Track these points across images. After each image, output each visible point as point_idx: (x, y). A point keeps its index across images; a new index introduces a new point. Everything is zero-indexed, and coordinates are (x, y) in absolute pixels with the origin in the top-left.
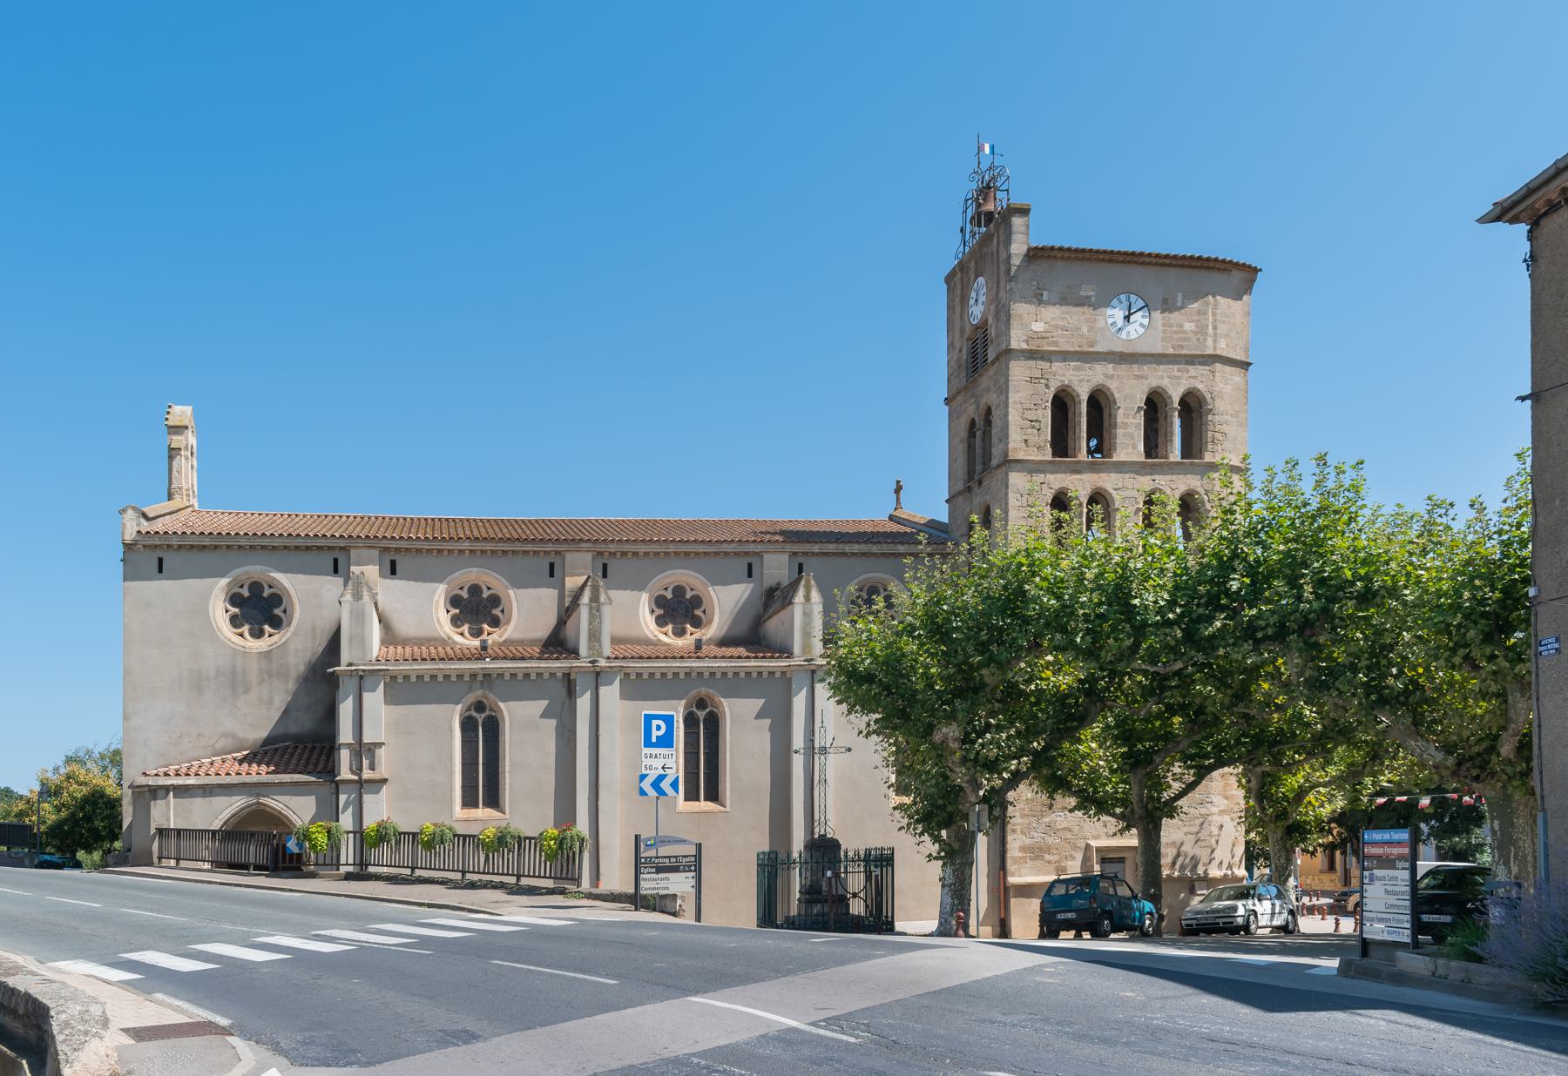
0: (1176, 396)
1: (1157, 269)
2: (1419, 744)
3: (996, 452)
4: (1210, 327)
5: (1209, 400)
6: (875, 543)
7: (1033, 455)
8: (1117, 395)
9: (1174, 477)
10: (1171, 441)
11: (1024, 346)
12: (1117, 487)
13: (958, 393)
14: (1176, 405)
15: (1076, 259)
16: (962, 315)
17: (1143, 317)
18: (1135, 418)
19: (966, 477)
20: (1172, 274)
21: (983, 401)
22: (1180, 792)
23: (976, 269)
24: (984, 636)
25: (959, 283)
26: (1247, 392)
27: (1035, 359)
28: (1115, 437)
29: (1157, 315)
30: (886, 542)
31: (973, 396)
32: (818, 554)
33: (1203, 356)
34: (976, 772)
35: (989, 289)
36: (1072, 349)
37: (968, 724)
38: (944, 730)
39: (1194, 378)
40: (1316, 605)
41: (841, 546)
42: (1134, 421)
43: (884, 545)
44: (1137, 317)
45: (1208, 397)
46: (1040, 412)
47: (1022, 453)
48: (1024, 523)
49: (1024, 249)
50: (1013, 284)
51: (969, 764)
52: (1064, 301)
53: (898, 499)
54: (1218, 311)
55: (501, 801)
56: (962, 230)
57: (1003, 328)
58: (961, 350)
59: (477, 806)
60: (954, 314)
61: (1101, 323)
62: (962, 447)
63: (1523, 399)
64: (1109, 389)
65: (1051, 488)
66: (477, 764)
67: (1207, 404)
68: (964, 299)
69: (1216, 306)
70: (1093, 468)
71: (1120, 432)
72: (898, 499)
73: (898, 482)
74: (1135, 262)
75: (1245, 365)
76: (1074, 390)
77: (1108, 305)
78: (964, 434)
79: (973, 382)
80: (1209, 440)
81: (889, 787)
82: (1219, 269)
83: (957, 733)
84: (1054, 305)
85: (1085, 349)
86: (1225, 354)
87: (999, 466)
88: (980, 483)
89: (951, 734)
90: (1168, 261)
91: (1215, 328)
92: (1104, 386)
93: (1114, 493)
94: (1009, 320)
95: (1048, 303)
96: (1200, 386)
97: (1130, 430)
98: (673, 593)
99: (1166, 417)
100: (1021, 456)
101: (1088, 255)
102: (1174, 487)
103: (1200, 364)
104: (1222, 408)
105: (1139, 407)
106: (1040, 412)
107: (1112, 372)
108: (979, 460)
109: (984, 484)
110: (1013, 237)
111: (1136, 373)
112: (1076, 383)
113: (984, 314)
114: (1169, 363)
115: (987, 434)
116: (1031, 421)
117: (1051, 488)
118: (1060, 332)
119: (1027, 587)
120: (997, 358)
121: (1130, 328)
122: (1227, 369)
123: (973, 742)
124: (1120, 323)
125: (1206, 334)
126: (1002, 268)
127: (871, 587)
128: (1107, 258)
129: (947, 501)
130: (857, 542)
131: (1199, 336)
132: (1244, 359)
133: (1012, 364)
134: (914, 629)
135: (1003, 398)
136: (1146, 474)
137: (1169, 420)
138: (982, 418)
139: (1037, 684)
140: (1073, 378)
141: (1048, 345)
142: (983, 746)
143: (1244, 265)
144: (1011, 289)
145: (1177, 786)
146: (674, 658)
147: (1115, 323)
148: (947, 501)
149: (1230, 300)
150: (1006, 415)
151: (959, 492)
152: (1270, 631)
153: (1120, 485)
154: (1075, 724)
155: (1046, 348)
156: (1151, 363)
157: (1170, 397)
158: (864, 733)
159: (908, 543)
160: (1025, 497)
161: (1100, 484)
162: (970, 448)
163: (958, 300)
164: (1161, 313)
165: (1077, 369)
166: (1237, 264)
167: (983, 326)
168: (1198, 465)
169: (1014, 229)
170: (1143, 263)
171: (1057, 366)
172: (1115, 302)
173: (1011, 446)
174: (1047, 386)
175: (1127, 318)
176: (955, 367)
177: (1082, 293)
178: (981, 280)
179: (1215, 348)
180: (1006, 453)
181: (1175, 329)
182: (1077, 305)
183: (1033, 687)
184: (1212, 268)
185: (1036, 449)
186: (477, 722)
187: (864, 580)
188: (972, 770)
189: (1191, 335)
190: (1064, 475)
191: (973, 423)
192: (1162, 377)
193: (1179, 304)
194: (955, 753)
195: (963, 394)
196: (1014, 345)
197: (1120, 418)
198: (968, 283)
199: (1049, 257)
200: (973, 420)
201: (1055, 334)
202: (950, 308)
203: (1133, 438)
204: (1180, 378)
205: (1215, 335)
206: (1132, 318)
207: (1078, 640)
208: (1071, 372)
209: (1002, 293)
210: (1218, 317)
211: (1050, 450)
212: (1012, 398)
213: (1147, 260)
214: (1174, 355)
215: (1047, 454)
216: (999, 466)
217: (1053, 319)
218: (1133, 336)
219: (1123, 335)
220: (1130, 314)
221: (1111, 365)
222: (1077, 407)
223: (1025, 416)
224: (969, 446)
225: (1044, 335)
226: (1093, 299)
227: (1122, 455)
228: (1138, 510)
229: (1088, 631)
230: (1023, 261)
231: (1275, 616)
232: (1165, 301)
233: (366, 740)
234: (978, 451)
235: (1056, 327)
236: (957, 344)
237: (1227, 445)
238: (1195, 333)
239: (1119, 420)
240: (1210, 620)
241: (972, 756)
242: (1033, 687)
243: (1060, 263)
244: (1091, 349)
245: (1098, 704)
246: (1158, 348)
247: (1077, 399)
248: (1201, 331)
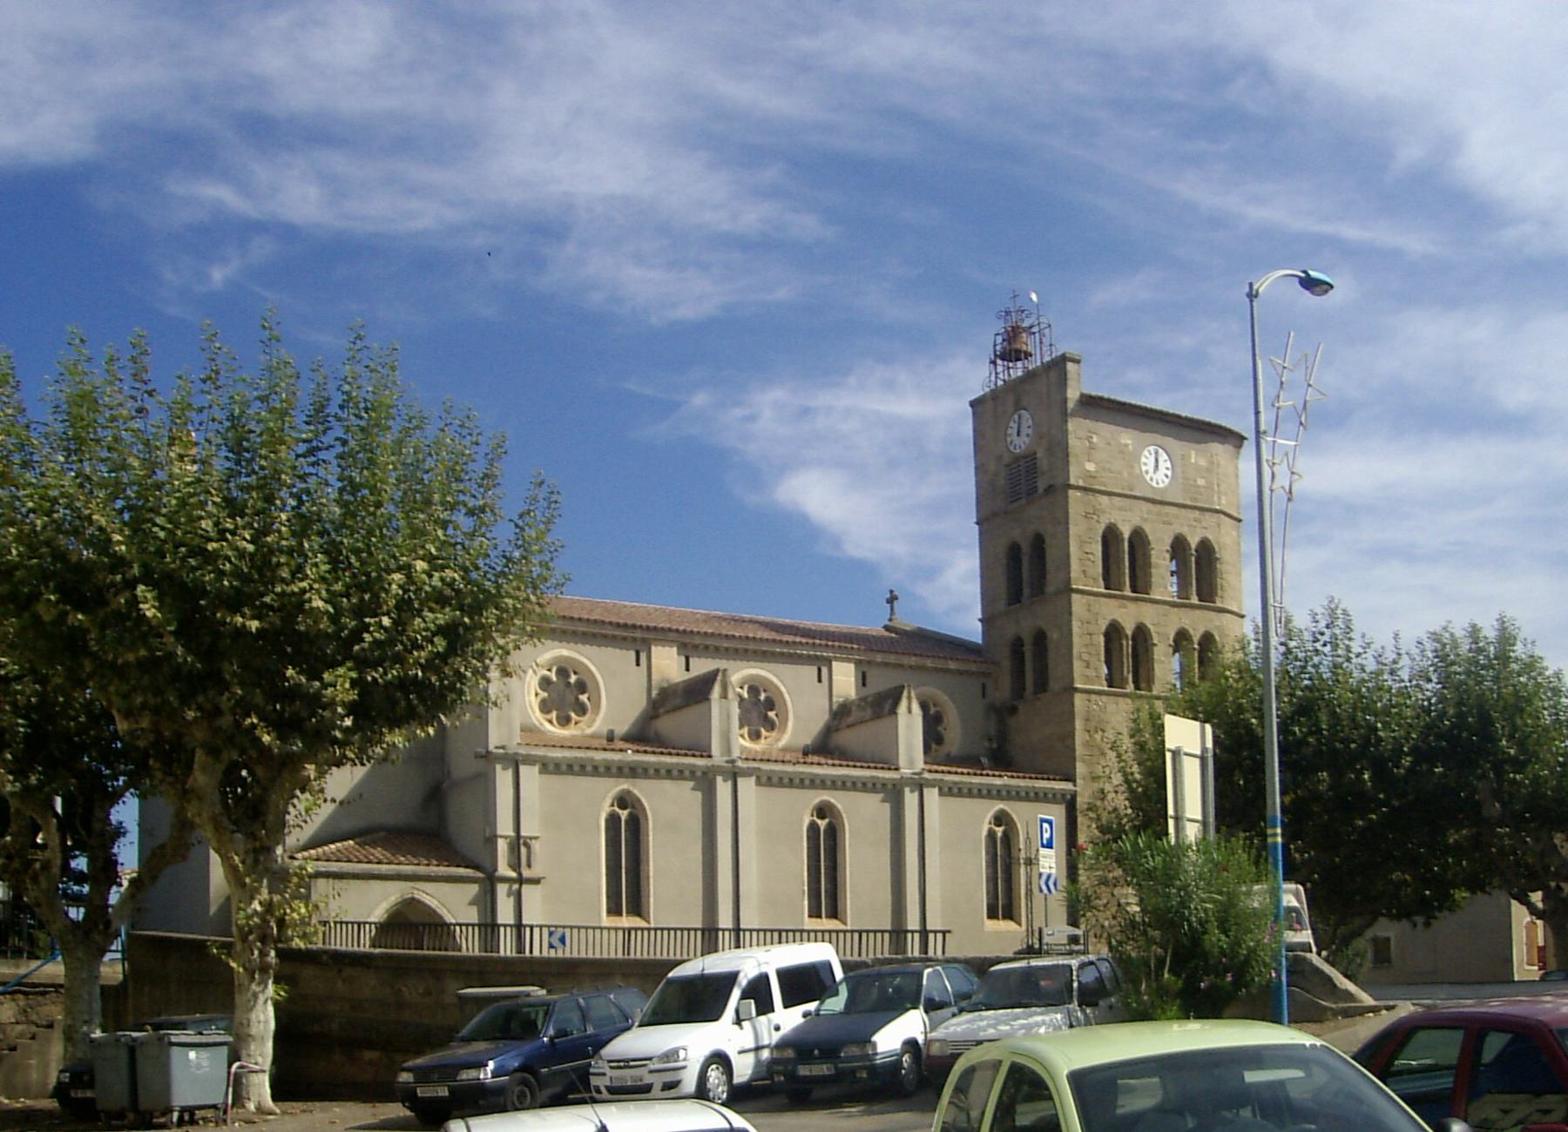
0: (1194, 542)
4: (1216, 486)
5: (1217, 550)
8: (1150, 537)
32: (879, 664)
45: (1216, 546)
53: (892, 609)
55: (644, 909)
59: (621, 915)
66: (621, 868)
72: (892, 609)
96: (1211, 537)
98: (544, 690)
106: (1093, 546)
125: (1213, 490)
146: (754, 760)
177: (1123, 441)
186: (620, 818)
204: (1195, 527)
212: (1073, 530)
230: (1076, 406)
233: (523, 833)
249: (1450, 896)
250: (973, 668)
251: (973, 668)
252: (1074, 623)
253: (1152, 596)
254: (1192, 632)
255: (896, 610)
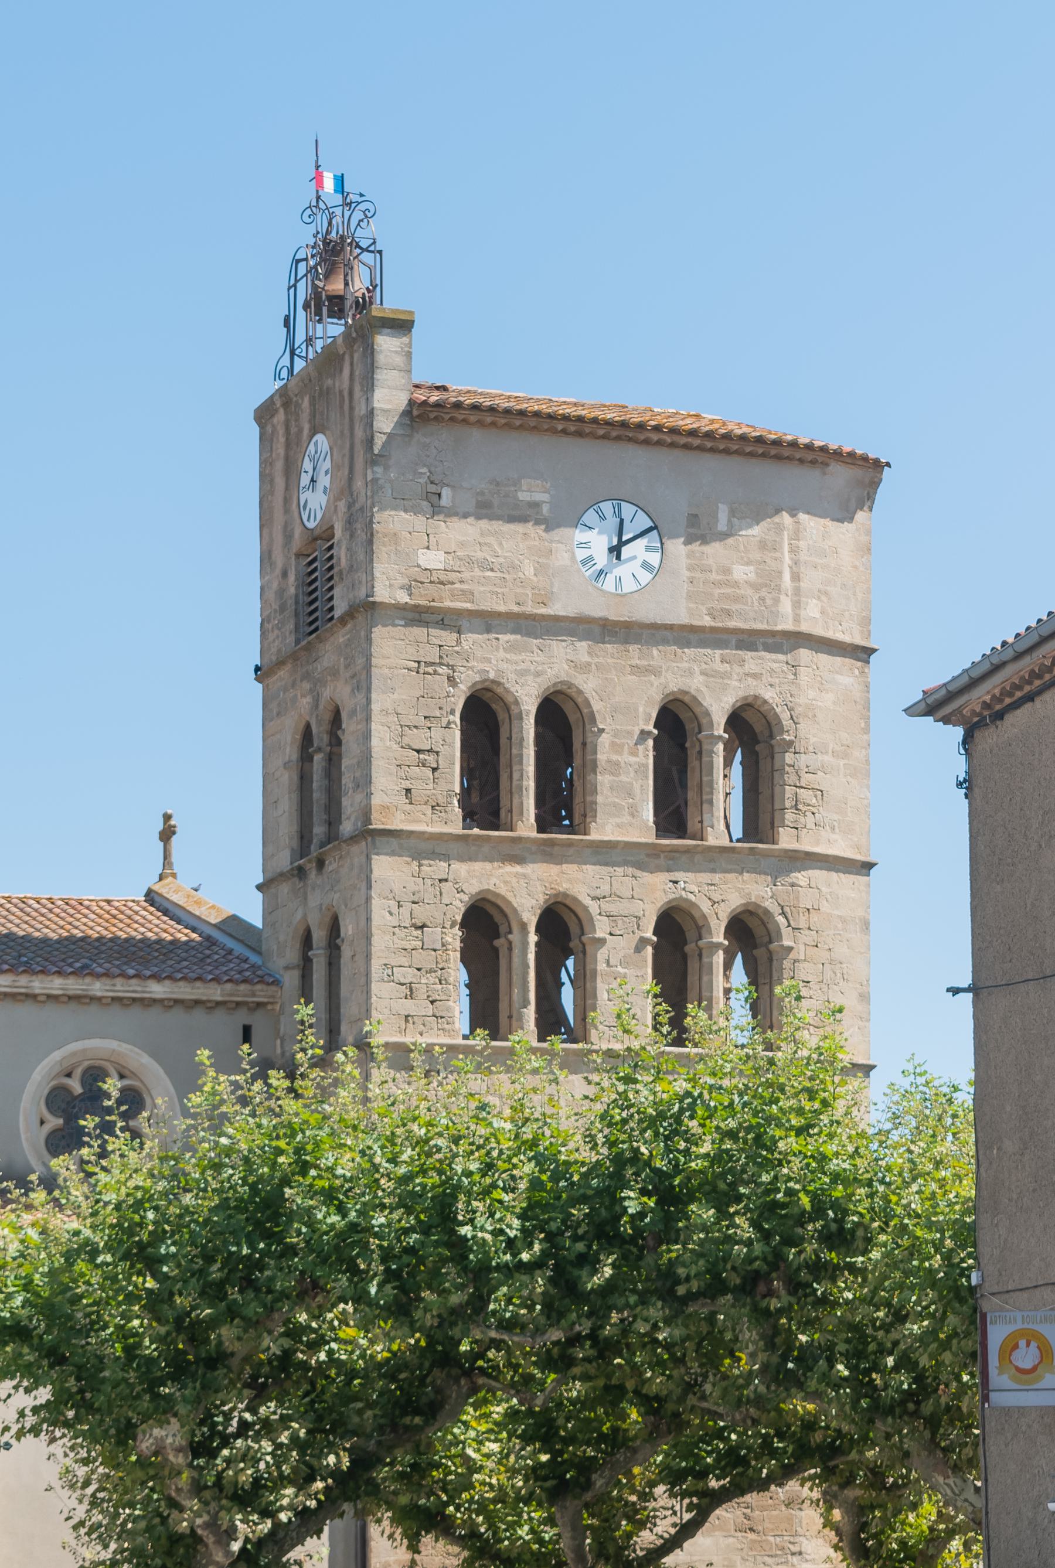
1: (677, 453)
2: (951, 1481)
3: (350, 804)
4: (787, 576)
5: (786, 723)
6: (98, 976)
7: (425, 823)
8: (596, 706)
9: (717, 877)
10: (711, 802)
11: (403, 598)
12: (598, 893)
13: (280, 663)
14: (719, 730)
15: (508, 426)
16: (287, 501)
17: (649, 549)
18: (634, 754)
19: (295, 843)
20: (709, 467)
21: (327, 693)
22: (666, 1541)
23: (313, 415)
24: (215, 1271)
25: (281, 431)
26: (867, 707)
27: (426, 624)
28: (595, 791)
29: (677, 547)
30: (124, 975)
31: (307, 676)
33: (773, 634)
34: (222, 1508)
35: (336, 467)
36: (502, 608)
37: (202, 1423)
38: (156, 1432)
39: (756, 676)
40: (758, 1248)
41: (23, 980)
42: (633, 759)
43: (119, 981)
44: (635, 550)
45: (785, 716)
46: (437, 733)
47: (399, 815)
48: (405, 961)
49: (401, 401)
50: (379, 470)
51: (207, 1494)
52: (484, 510)
53: (167, 856)
54: (802, 544)
56: (286, 323)
57: (361, 557)
58: (285, 574)
60: (272, 492)
61: (561, 559)
62: (287, 779)
63: (955, 991)
64: (580, 692)
65: (460, 891)
67: (782, 731)
68: (292, 470)
69: (797, 535)
70: (548, 854)
71: (603, 780)
72: (167, 856)
73: (167, 817)
74: (630, 440)
75: (863, 653)
76: (507, 690)
77: (576, 522)
78: (291, 752)
79: (308, 648)
80: (788, 804)
81: (75, 1528)
82: (801, 461)
83: (178, 1438)
84: (465, 516)
85: (530, 608)
86: (819, 631)
87: (353, 839)
88: (321, 864)
89: (170, 1440)
90: (696, 442)
91: (796, 577)
92: (570, 685)
93: (593, 907)
94: (370, 542)
95: (451, 513)
96: (769, 695)
97: (623, 778)
99: (700, 753)
100: (397, 823)
101: (533, 422)
102: (716, 897)
103: (769, 649)
104: (813, 740)
105: (642, 732)
106: (437, 733)
107: (586, 658)
108: (319, 816)
109: (330, 866)
110: (380, 376)
111: (636, 662)
112: (512, 677)
113: (331, 509)
114: (703, 644)
115: (333, 760)
116: (418, 751)
117: (460, 891)
118: (477, 572)
119: (288, 1192)
120: (350, 614)
121: (623, 571)
122: (824, 659)
123: (213, 1454)
124: (602, 558)
126: (359, 433)
127: (90, 1068)
128: (573, 429)
129: (259, 887)
130: (59, 973)
131: (763, 593)
132: (859, 641)
133: (378, 632)
134: (94, 1253)
135: (360, 697)
136: (658, 869)
137: (705, 759)
138: (325, 727)
139: (330, 1353)
140: (504, 666)
141: (453, 596)
142: (228, 1461)
143: (852, 455)
144: (375, 480)
145: (665, 1527)
147: (590, 558)
148: (259, 887)
149: (828, 522)
150: (367, 736)
151: (282, 874)
152: (695, 1286)
153: (605, 889)
154: (417, 1420)
155: (448, 604)
156: (665, 642)
157: (708, 714)
158: (13, 1431)
159: (169, 977)
160: (407, 907)
161: (564, 887)
162: (304, 779)
163: (279, 465)
164: (686, 543)
165: (512, 648)
166: (838, 454)
167: (324, 536)
168: (766, 854)
169: (381, 359)
170: (647, 442)
171: (471, 640)
172: (590, 516)
173: (376, 800)
174: (451, 680)
175: (616, 551)
176: (276, 606)
177: (523, 496)
178: (320, 438)
179: (797, 619)
180: (366, 815)
181: (714, 576)
182: (512, 519)
183: (323, 1356)
184: (789, 458)
185: (429, 811)
187: (74, 1054)
188: (213, 1505)
189: (749, 592)
190: (488, 866)
191: (307, 735)
192: (690, 673)
193: (722, 526)
194: (179, 1473)
195: (288, 666)
196: (382, 593)
197: (604, 750)
198: (298, 444)
199: (452, 419)
200: (308, 727)
201: (466, 575)
202: (265, 477)
203: (630, 795)
205: (797, 592)
206: (626, 552)
207: (373, 1290)
208: (501, 654)
209: (359, 483)
210: (803, 556)
211: (458, 811)
212: (380, 702)
213: (655, 437)
214: (713, 630)
215: (452, 822)
216: (353, 839)
217: (462, 545)
218: (629, 586)
219: (609, 584)
220: (621, 544)
221: (584, 644)
222: (515, 722)
223: (406, 740)
224: (302, 778)
225: (443, 577)
226: (545, 509)
227: (609, 828)
228: (643, 942)
229: (390, 1276)
230: (398, 424)
231: (701, 1262)
232: (693, 520)
234: (318, 795)
235: (470, 562)
236: (279, 560)
237: (826, 814)
238: (756, 587)
239: (602, 757)
240: (592, 1263)
241: (210, 1481)
242: (323, 1356)
243: (476, 434)
244: (543, 611)
245: (463, 1382)
246: (680, 614)
247: (514, 710)
248: (768, 582)
249: (887, 1416)
250: (215, 993)
251: (215, 993)
252: (376, 903)
253: (594, 836)
254: (705, 906)
255: (175, 858)
